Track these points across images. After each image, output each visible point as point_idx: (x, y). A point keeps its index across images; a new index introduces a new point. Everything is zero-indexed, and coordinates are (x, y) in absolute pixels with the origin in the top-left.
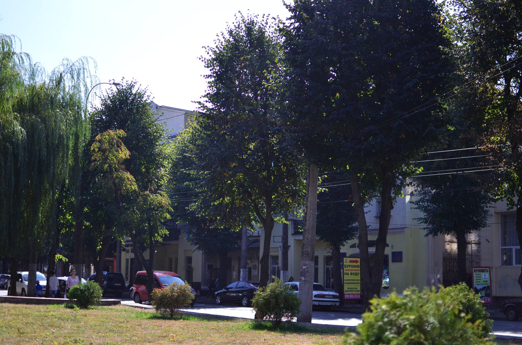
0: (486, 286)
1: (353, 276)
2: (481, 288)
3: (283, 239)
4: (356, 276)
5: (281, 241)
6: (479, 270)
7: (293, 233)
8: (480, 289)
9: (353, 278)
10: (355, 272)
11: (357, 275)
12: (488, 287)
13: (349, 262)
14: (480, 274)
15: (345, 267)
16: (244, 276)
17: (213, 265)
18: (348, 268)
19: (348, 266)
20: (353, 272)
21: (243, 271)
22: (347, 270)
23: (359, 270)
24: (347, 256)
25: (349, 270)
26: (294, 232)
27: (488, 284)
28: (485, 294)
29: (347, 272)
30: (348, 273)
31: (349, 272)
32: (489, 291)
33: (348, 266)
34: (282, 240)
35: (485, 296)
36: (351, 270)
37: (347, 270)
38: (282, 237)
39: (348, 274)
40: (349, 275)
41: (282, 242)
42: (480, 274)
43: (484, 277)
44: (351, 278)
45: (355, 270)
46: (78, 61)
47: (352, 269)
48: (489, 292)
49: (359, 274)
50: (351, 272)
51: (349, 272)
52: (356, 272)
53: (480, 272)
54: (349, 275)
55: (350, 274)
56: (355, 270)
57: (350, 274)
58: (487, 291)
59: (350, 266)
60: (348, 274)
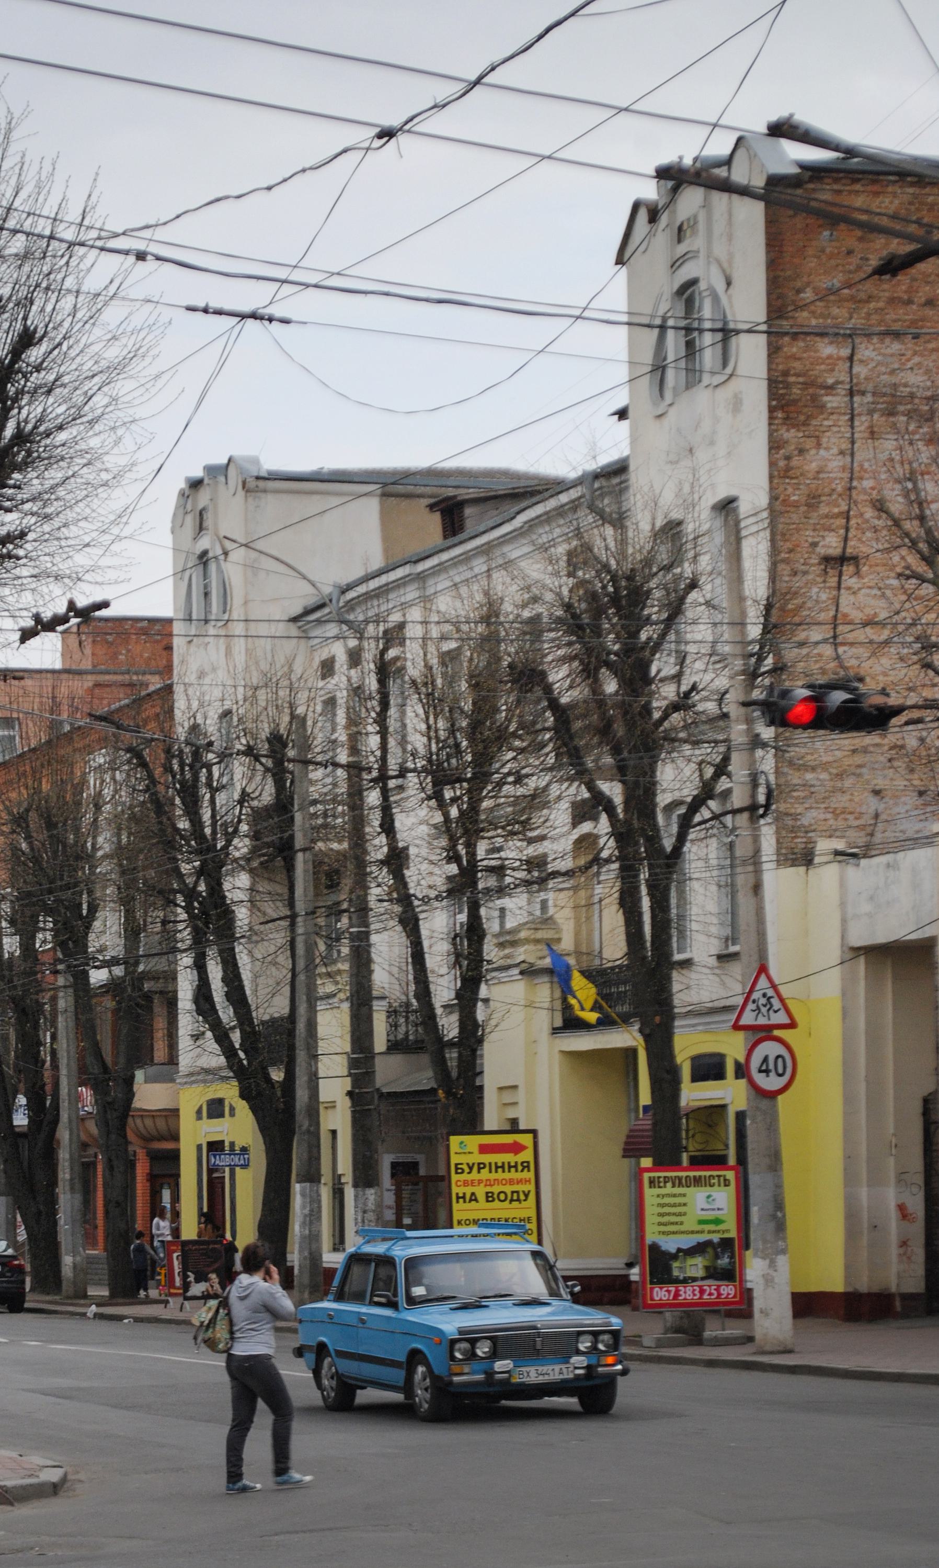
0: (716, 1238)
1: (497, 1203)
2: (685, 1247)
3: (353, 1064)
4: (515, 1204)
5: (346, 1073)
6: (680, 1179)
7: (559, 1023)
8: (679, 1250)
9: (496, 1215)
10: (508, 1189)
11: (518, 1200)
12: (726, 1244)
13: (476, 1150)
14: (684, 1195)
15: (461, 1172)
16: (307, 1211)
17: (415, 1165)
18: (475, 1175)
19: (471, 1168)
20: (496, 1189)
21: (303, 1195)
22: (466, 1183)
23: (528, 1181)
24: (487, 1127)
25: (480, 1182)
26: (564, 1021)
27: (728, 1231)
28: (707, 1268)
29: (468, 1191)
30: (473, 1194)
31: (480, 1192)
32: (732, 1257)
33: (471, 1168)
34: (350, 1068)
35: (703, 1279)
36: (489, 1183)
37: (466, 1183)
38: (349, 1057)
39: (474, 1198)
40: (476, 1200)
41: (350, 1075)
42: (684, 1195)
43: (707, 1206)
44: (489, 1215)
45: (511, 1182)
46: (81, 298)
47: (493, 1176)
48: (732, 1264)
49: (527, 1195)
50: (489, 1189)
51: (480, 1192)
52: (515, 1188)
53: (680, 1184)
54: (476, 1200)
55: (481, 1196)
56: (511, 1182)
57: (481, 1196)
58: (717, 1257)
59: (481, 1166)
60: (474, 1198)
